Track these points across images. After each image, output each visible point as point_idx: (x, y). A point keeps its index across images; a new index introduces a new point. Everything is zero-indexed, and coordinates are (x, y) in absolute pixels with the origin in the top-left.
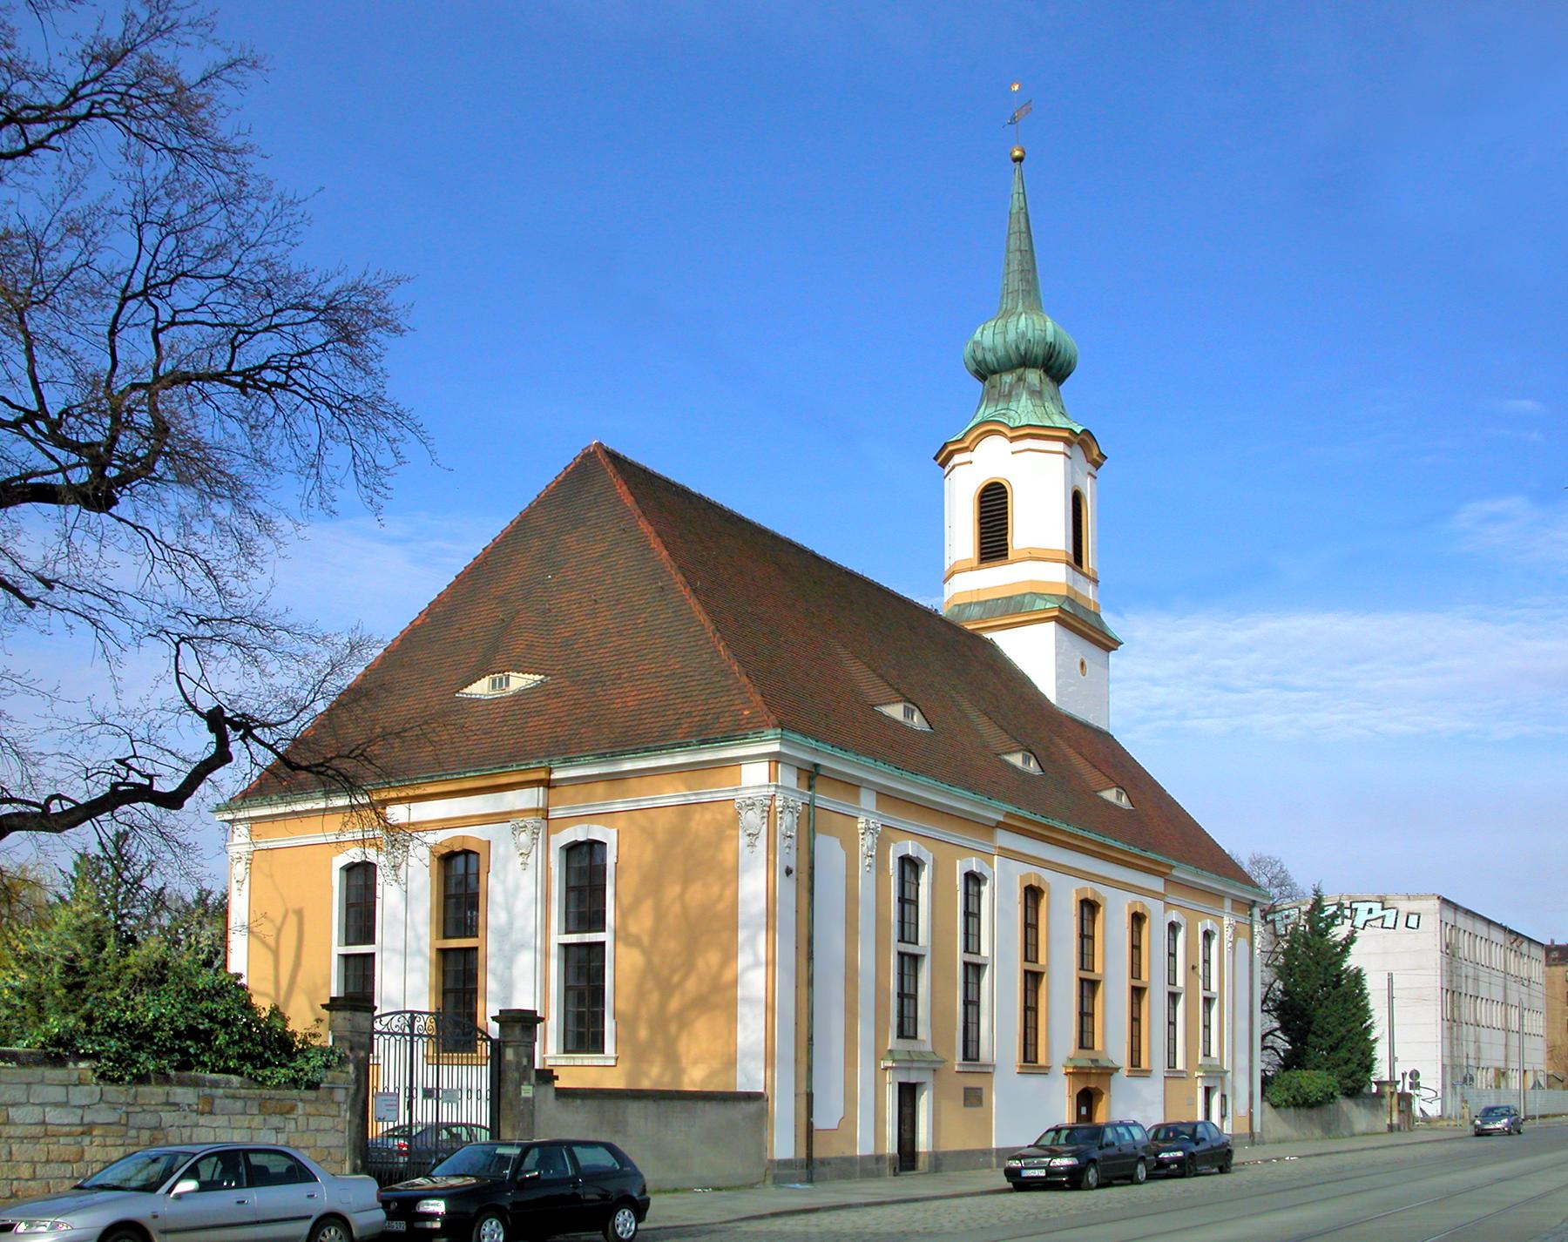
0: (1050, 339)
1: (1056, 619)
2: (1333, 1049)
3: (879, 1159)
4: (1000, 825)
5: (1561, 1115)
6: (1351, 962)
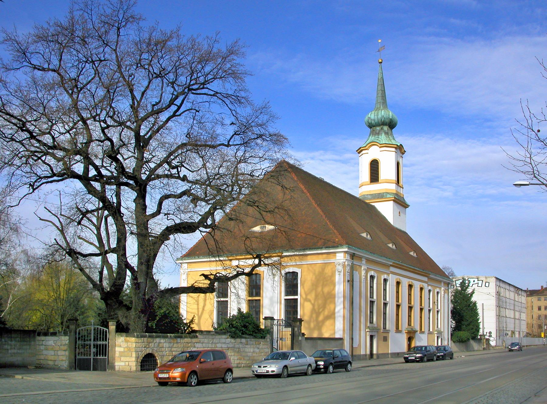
0: (391, 117)
1: (394, 201)
2: (469, 325)
3: (366, 355)
4: (391, 265)
5: (531, 346)
6: (473, 299)
